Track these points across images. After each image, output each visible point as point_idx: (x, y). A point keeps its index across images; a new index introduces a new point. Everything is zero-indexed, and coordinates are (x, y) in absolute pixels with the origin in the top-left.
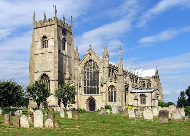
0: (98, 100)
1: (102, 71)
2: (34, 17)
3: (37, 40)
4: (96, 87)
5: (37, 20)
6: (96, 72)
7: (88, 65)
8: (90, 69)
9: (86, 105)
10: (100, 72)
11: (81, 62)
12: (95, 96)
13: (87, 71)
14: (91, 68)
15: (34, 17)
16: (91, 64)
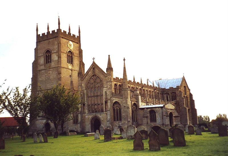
0: (103, 119)
1: (106, 86)
5: (40, 33)
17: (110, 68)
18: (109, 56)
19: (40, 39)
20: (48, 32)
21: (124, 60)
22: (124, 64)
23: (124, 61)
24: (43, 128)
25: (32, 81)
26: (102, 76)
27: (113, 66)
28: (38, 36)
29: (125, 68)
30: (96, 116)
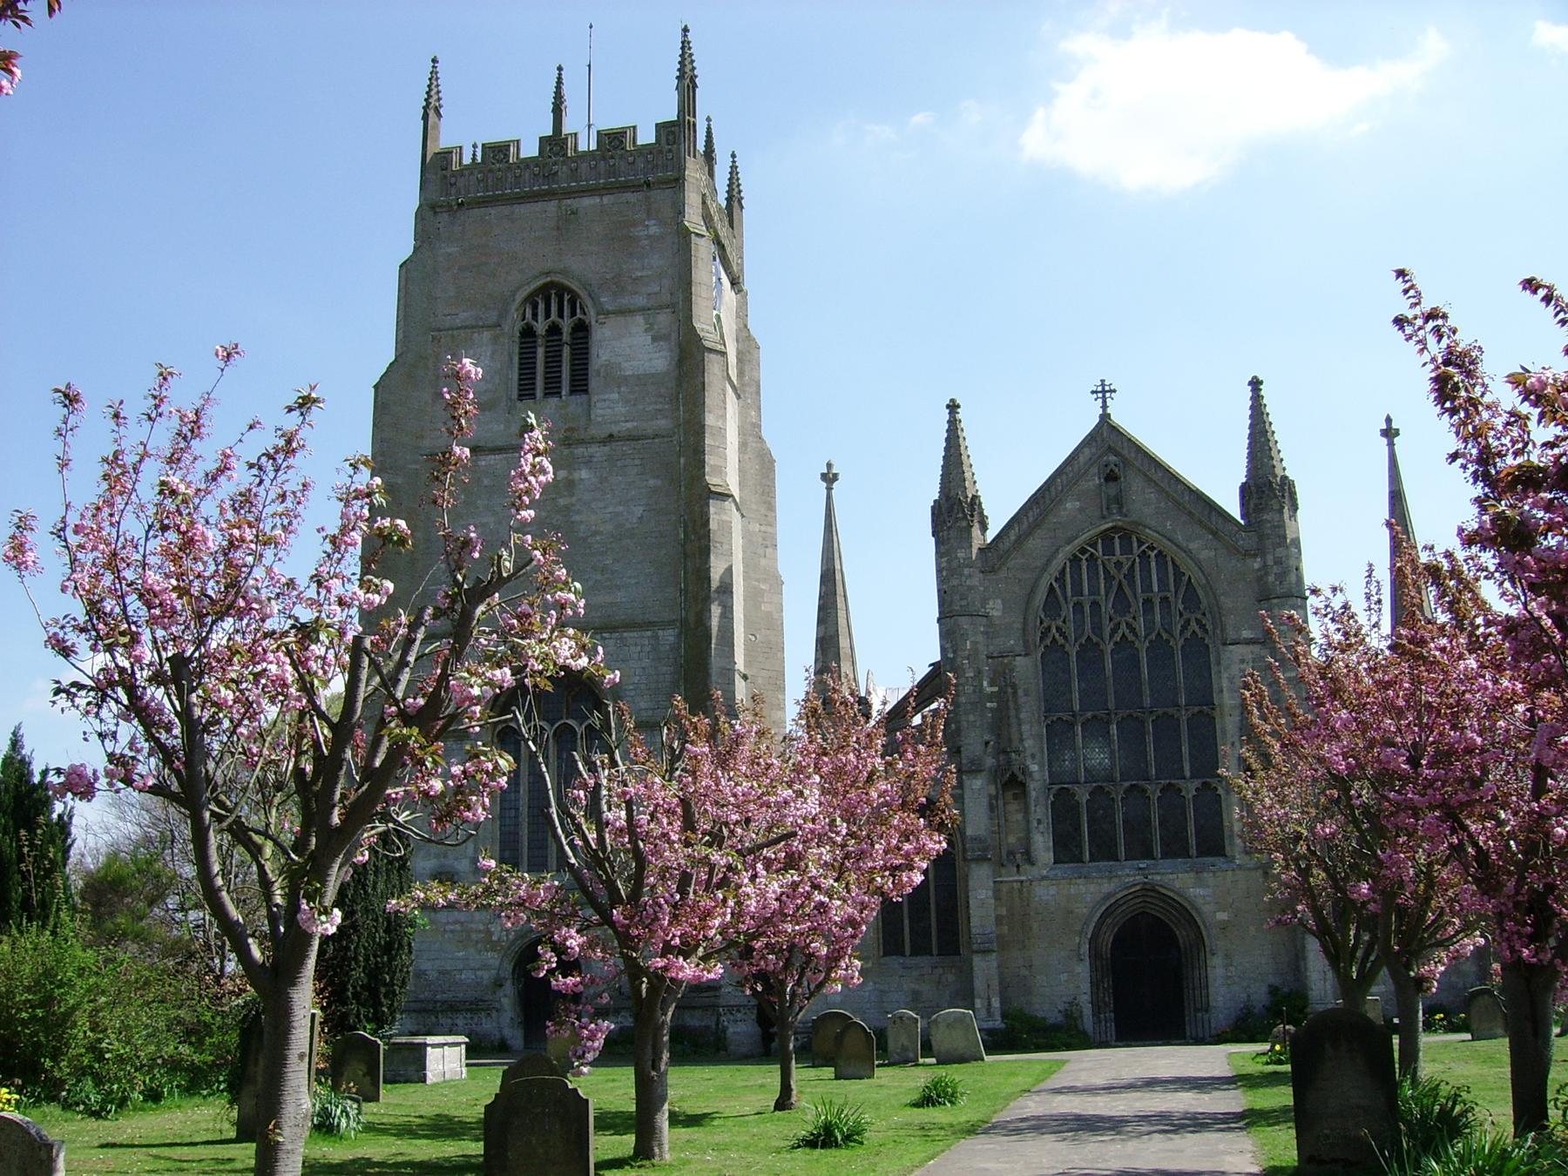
0: (1222, 916)
1: (1246, 634)
2: (431, 110)
3: (464, 316)
4: (1190, 788)
5: (465, 134)
6: (1178, 644)
7: (1093, 576)
8: (1107, 608)
9: (1083, 970)
10: (1231, 635)
11: (443, 1045)
12: (1183, 880)
13: (1079, 625)
14: (1122, 604)
15: (431, 110)
16: (1118, 565)
17: (1268, 490)
18: (1255, 384)
19: (462, 193)
20: (555, 143)
21: (1389, 433)
22: (829, 497)
23: (829, 489)
24: (498, 984)
25: (704, 461)
26: (1202, 548)
27: (1293, 461)
28: (438, 169)
29: (1397, 498)
30: (1149, 890)
